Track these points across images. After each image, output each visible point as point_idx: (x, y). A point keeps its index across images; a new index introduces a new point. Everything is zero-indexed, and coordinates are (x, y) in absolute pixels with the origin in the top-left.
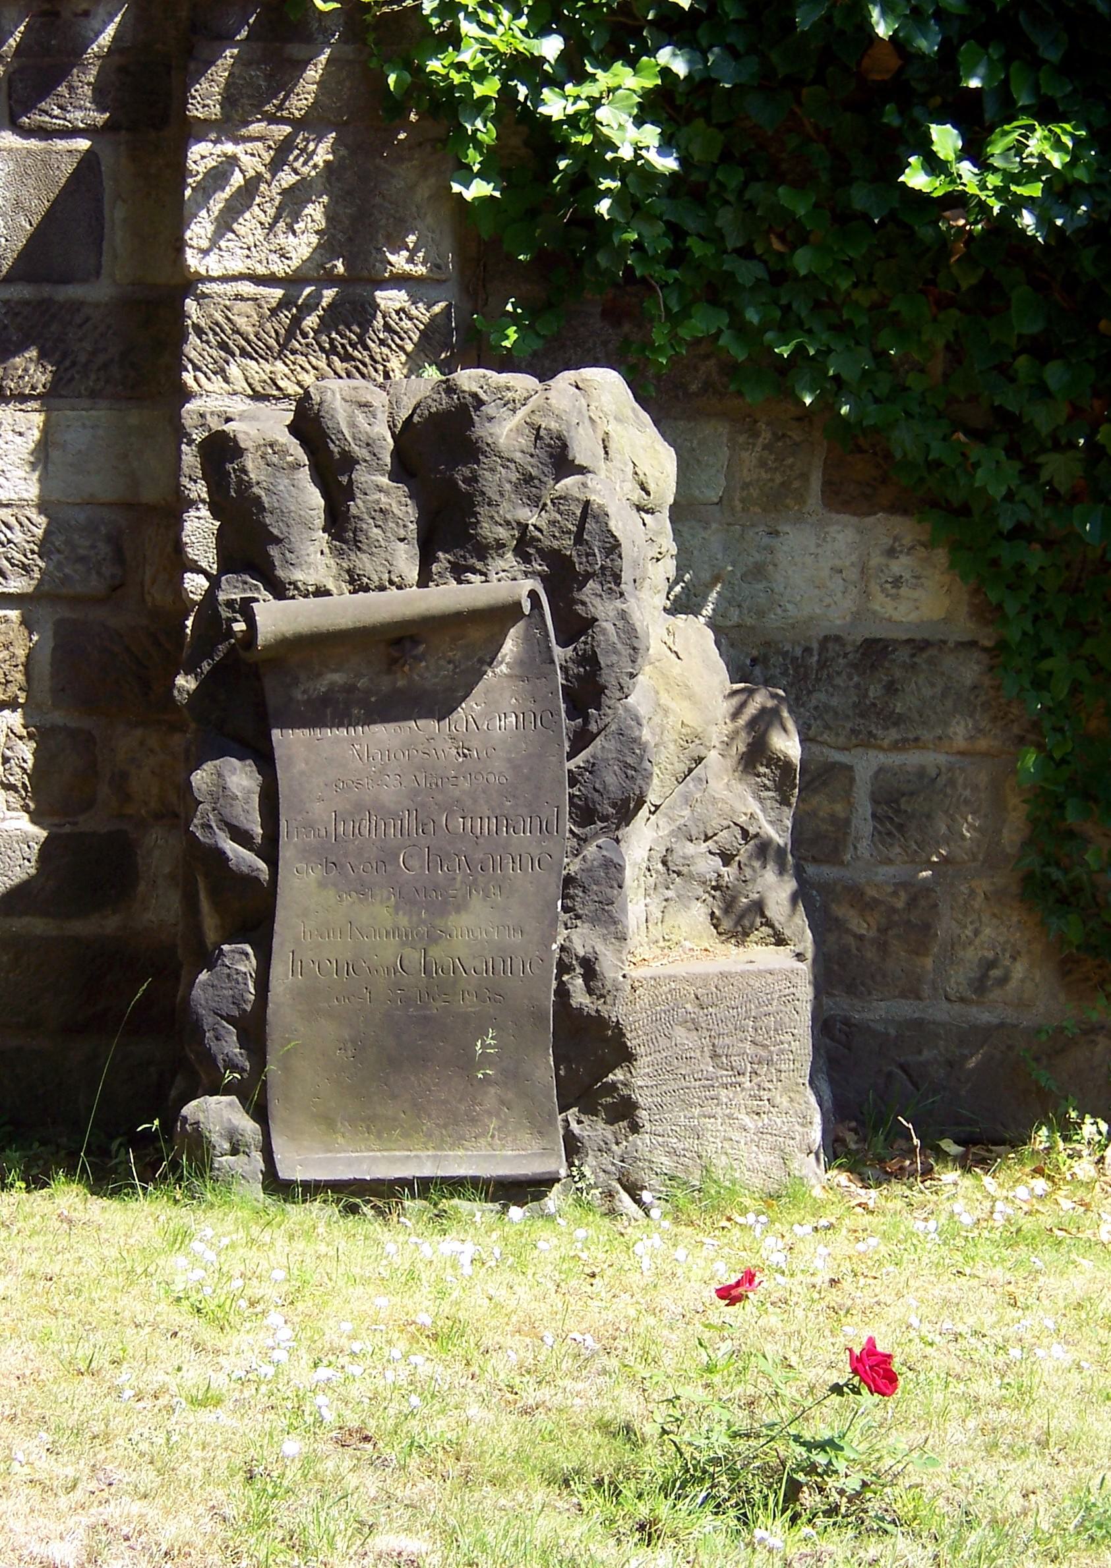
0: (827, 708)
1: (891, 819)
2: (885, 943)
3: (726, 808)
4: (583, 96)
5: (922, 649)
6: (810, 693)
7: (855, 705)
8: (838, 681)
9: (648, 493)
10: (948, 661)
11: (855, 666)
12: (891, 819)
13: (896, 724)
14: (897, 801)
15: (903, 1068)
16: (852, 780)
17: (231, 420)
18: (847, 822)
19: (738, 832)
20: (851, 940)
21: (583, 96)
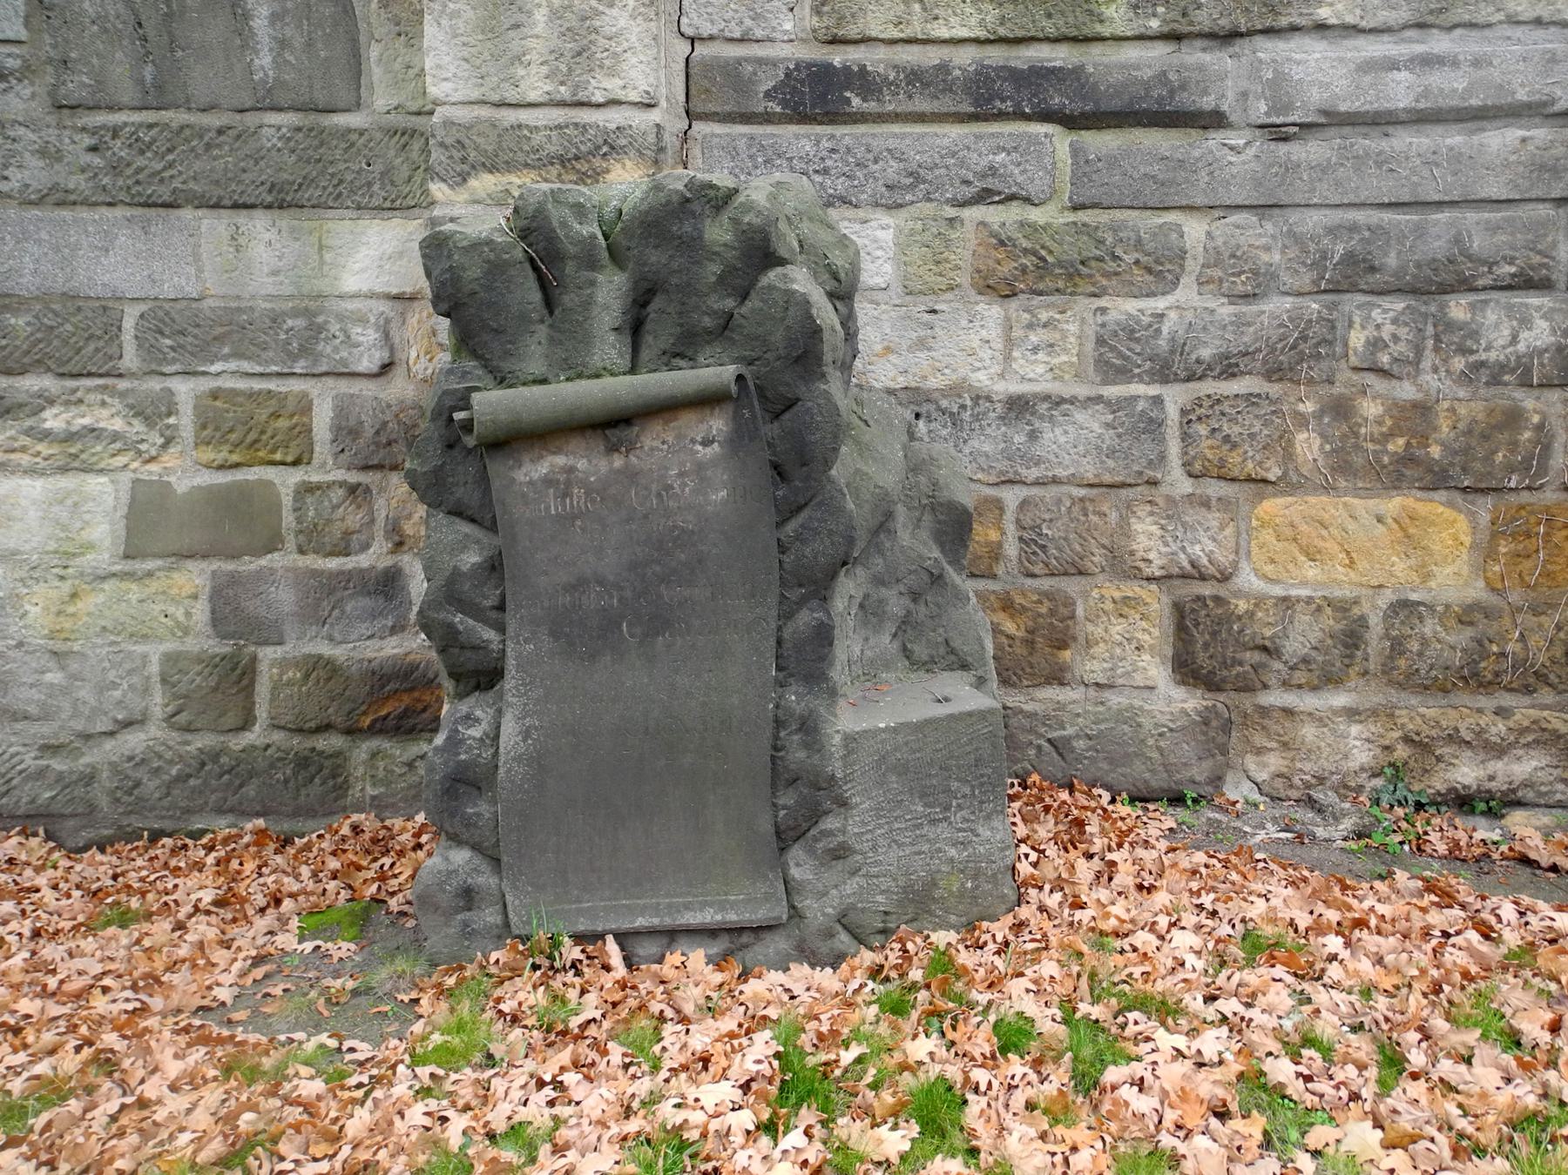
0: (980, 454)
1: (1036, 543)
2: (1033, 642)
3: (913, 555)
4: (1465, 68)
5: (1058, 404)
6: (965, 442)
7: (1003, 451)
8: (988, 431)
9: (839, 281)
10: (1080, 416)
11: (1000, 418)
12: (1036, 543)
13: (1036, 464)
14: (1039, 527)
15: (1049, 741)
16: (1002, 510)
17: (403, 1117)
18: (1000, 545)
19: (926, 578)
20: (1004, 640)
21: (1465, 68)
